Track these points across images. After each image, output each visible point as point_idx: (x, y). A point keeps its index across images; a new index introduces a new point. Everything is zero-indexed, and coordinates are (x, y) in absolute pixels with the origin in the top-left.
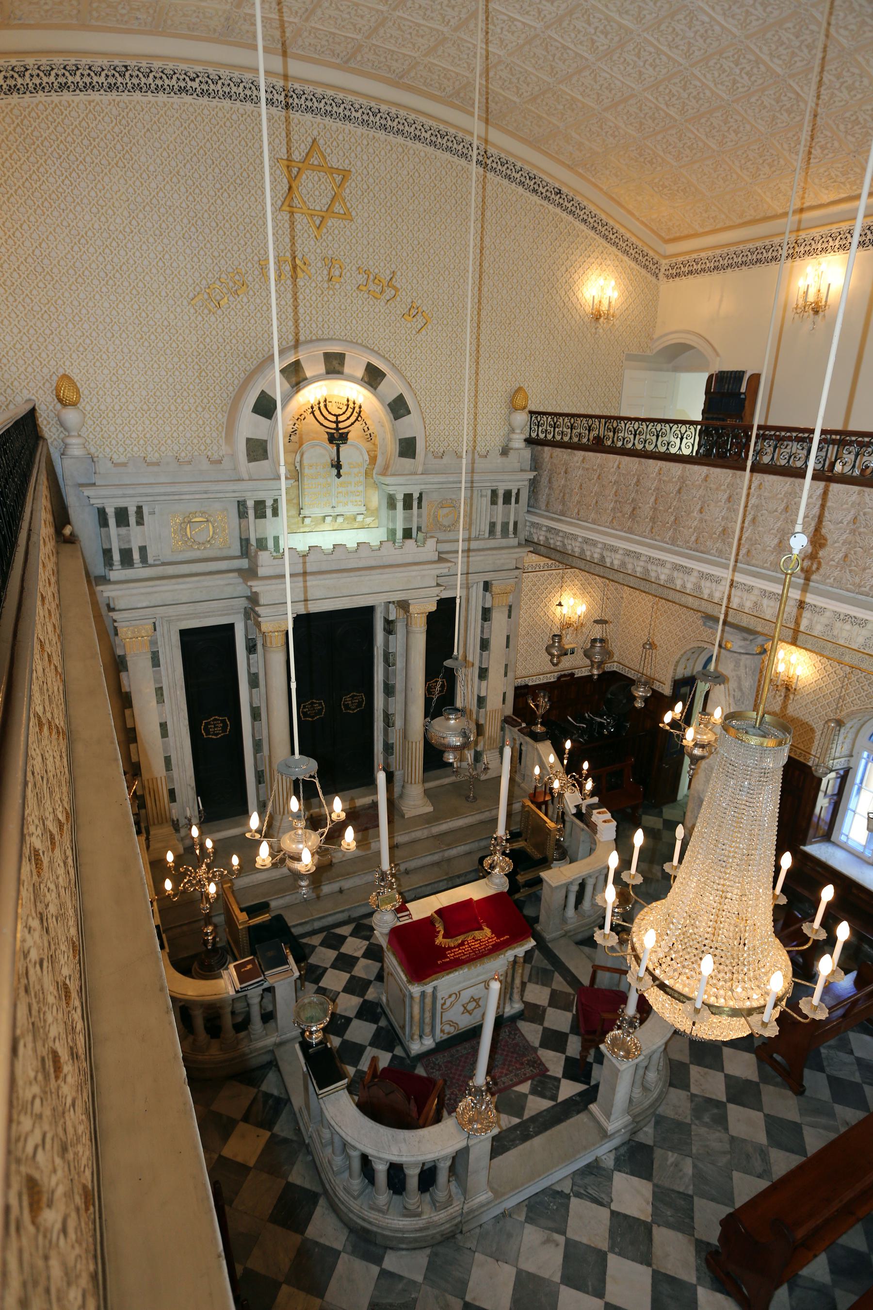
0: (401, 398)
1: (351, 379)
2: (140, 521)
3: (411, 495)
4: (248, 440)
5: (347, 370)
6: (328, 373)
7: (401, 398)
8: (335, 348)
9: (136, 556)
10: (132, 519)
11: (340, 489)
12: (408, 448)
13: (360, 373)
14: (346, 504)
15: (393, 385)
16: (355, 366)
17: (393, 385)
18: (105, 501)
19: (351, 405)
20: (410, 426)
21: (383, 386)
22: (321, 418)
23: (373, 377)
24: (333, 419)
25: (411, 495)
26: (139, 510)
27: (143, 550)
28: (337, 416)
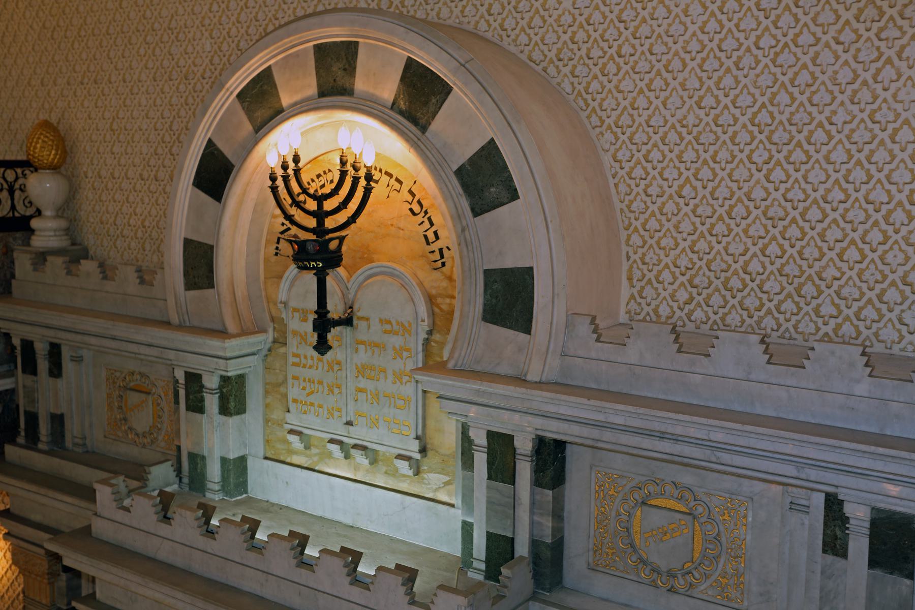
0: (490, 151)
1: (368, 106)
2: (56, 370)
3: (224, 410)
4: (187, 242)
5: (360, 84)
6: (322, 94)
7: (490, 151)
8: (335, 33)
9: (44, 429)
10: (43, 365)
11: (363, 383)
12: (509, 298)
13: (388, 89)
14: (374, 424)
15: (466, 122)
16: (380, 78)
17: (466, 122)
18: (13, 326)
19: (351, 172)
20: (521, 234)
21: (443, 123)
22: (353, 206)
23: (419, 100)
24: (312, 205)
25: (224, 410)
26: (55, 351)
27: (58, 420)
28: (320, 199)
